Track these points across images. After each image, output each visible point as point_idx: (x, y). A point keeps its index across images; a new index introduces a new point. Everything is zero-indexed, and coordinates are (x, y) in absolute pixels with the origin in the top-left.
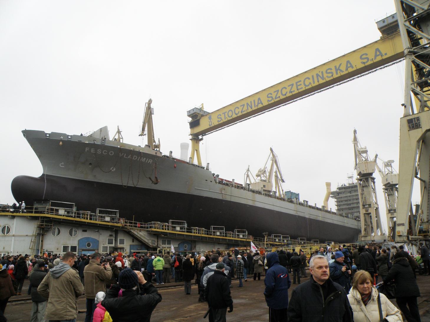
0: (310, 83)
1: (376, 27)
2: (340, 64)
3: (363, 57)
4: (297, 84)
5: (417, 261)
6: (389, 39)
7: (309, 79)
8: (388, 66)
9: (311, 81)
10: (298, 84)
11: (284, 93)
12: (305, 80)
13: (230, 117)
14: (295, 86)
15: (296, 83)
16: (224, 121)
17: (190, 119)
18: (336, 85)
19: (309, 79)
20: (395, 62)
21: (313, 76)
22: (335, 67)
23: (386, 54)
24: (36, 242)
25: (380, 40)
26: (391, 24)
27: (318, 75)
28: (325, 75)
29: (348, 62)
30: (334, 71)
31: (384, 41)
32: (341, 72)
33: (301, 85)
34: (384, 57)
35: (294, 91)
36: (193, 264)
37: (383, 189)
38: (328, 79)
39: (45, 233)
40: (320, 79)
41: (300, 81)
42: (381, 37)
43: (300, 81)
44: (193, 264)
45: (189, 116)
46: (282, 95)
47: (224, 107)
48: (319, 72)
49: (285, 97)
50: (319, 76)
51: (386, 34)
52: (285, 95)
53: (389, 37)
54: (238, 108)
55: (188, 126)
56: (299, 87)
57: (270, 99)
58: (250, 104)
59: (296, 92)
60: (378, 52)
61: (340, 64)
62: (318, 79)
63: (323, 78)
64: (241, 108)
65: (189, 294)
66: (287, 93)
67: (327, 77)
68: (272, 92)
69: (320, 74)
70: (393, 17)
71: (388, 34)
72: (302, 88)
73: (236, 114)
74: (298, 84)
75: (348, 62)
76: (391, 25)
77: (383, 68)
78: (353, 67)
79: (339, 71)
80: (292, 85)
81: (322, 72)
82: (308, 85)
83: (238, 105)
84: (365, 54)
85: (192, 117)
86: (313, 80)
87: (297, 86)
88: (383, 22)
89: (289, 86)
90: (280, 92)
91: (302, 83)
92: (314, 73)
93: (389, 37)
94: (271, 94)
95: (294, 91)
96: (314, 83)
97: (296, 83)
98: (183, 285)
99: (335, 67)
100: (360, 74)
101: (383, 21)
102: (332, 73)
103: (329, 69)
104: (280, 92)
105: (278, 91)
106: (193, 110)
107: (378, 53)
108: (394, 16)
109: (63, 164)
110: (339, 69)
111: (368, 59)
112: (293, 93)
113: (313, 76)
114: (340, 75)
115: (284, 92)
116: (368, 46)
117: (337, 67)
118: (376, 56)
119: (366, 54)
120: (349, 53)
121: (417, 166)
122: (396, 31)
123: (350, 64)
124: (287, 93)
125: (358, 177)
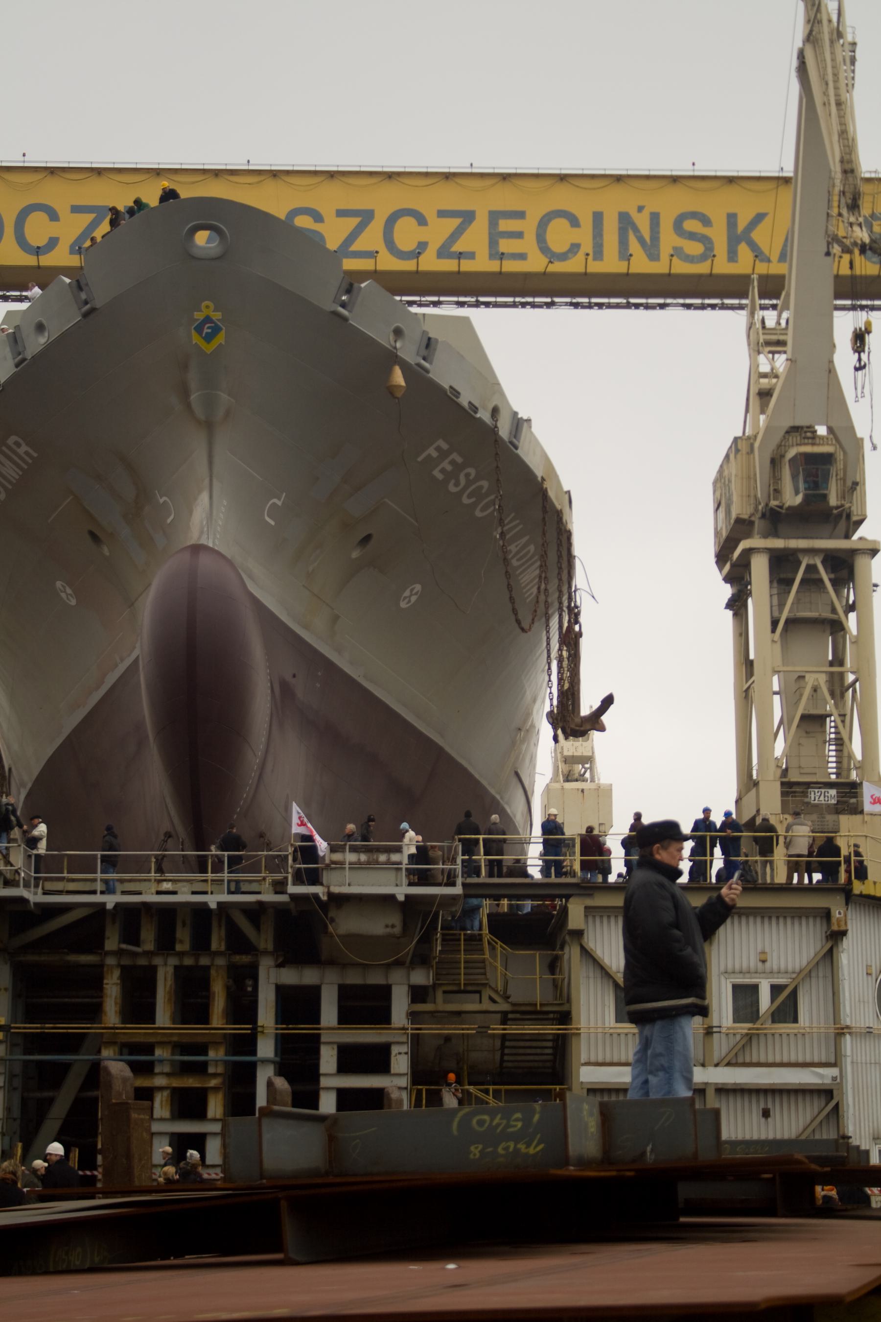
0: (575, 248)
2: (759, 218)
4: (497, 224)
5: (858, 887)
7: (574, 222)
9: (584, 236)
10: (505, 225)
11: (36, 238)
12: (549, 221)
14: (481, 225)
15: (495, 217)
16: (717, 270)
19: (574, 222)
20: (530, 300)
21: (598, 218)
22: (732, 219)
27: (626, 222)
28: (668, 240)
30: (719, 235)
32: (675, 259)
33: (519, 235)
35: (471, 256)
38: (681, 268)
40: (634, 246)
41: (520, 215)
43: (520, 215)
46: (544, 249)
48: (640, 209)
50: (636, 230)
52: (38, 251)
54: (422, 220)
56: (505, 246)
58: (643, 222)
59: (482, 264)
61: (759, 218)
62: (623, 243)
63: (652, 250)
64: (438, 231)
66: (53, 243)
67: (677, 252)
68: (327, 210)
69: (643, 222)
72: (522, 257)
73: (553, 257)
74: (505, 225)
77: (584, 307)
79: (743, 250)
80: (468, 217)
81: (655, 218)
82: (563, 257)
83: (430, 201)
84: (704, 215)
86: (594, 237)
87: (494, 237)
89: (341, 213)
90: (376, 229)
91: (529, 226)
92: (612, 204)
94: (318, 217)
95: (471, 256)
96: (598, 253)
97: (495, 217)
99: (732, 219)
100: (703, 297)
102: (706, 241)
103: (694, 215)
104: (376, 229)
105: (367, 216)
109: (818, 1188)
110: (746, 237)
112: (467, 266)
113: (598, 218)
115: (407, 234)
117: (741, 225)
121: (553, 614)
124: (53, 243)
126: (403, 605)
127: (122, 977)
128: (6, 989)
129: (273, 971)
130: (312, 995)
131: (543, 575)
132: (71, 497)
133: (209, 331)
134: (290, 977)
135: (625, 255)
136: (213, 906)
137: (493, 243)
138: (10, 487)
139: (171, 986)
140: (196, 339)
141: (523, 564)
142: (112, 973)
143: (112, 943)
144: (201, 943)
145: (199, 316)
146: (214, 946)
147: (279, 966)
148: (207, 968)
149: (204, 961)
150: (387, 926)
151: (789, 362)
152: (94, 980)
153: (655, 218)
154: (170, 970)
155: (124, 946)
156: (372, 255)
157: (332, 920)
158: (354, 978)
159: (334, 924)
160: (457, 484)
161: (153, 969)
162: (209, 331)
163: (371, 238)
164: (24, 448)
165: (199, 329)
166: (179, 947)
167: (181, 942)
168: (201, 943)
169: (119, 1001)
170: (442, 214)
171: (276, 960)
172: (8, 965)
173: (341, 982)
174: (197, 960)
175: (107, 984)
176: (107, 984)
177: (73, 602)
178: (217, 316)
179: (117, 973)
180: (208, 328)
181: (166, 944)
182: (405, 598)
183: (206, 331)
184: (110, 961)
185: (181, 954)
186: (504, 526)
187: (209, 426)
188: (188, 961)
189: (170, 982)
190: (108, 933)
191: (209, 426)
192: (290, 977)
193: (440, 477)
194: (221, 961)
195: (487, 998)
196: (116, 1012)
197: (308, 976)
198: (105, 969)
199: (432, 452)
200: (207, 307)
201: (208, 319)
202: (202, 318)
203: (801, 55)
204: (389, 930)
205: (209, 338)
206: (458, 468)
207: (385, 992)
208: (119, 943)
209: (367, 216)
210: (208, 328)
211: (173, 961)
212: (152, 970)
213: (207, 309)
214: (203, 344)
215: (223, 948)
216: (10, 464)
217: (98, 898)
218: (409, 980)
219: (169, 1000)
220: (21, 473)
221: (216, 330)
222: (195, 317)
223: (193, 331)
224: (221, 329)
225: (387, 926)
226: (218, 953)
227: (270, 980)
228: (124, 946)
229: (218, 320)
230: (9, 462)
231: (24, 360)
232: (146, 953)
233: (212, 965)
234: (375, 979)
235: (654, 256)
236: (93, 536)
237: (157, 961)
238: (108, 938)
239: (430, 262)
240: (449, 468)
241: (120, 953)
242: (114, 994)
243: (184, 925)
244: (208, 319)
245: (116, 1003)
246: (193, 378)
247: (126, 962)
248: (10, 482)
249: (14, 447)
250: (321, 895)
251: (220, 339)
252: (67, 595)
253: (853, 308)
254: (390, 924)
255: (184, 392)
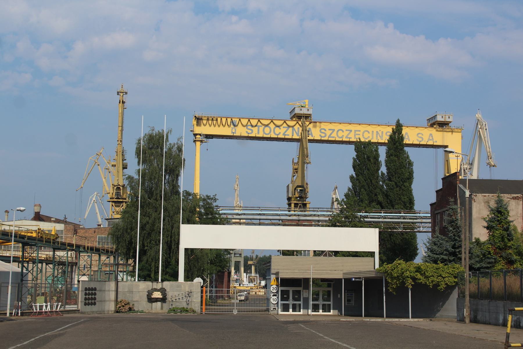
3: (420, 135)
7: (369, 132)
9: (370, 135)
10: (357, 133)
13: (339, 137)
14: (353, 131)
19: (369, 132)
21: (373, 132)
23: (436, 142)
24: (439, 211)
27: (377, 132)
35: (288, 135)
37: (354, 158)
40: (379, 138)
41: (360, 131)
43: (360, 131)
49: (276, 136)
52: (341, 137)
54: (343, 131)
57: (323, 135)
58: (380, 133)
62: (377, 136)
65: (486, 202)
66: (280, 133)
69: (380, 133)
74: (357, 133)
80: (351, 131)
81: (382, 132)
82: (367, 139)
89: (329, 130)
91: (361, 133)
94: (325, 130)
95: (288, 135)
96: (258, 133)
97: (355, 131)
107: (431, 138)
113: (373, 132)
115: (340, 134)
118: (429, 140)
119: (422, 135)
124: (280, 133)
125: (355, 157)
131: (69, 286)
135: (377, 138)
137: (355, 136)
151: (103, 289)
153: (382, 132)
156: (334, 137)
163: (334, 134)
170: (346, 130)
186: (127, 274)
203: (288, 186)
209: (334, 130)
235: (382, 139)
239: (345, 139)
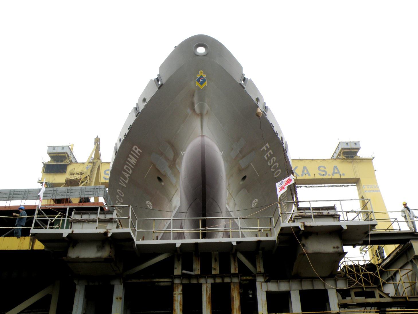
1: (46, 150)
2: (296, 167)
3: (321, 168)
6: (348, 162)
8: (336, 187)
17: (48, 159)
18: (329, 186)
25: (329, 159)
26: (59, 153)
29: (305, 168)
31: (343, 162)
34: (342, 177)
36: (339, 269)
39: (416, 260)
42: (48, 161)
44: (339, 269)
45: (49, 153)
47: (301, 160)
51: (54, 161)
53: (348, 160)
55: (40, 167)
60: (305, 170)
61: (296, 167)
70: (63, 148)
71: (347, 157)
75: (305, 168)
76: (60, 155)
78: (309, 175)
85: (52, 157)
88: (61, 148)
93: (348, 160)
98: (29, 248)
101: (54, 148)
106: (63, 148)
107: (336, 171)
108: (55, 148)
111: (326, 173)
114: (313, 178)
116: (327, 161)
119: (325, 168)
120: (295, 160)
122: (62, 162)
123: (307, 170)
126: (253, 206)
127: (183, 290)
128: (121, 298)
129: (264, 285)
130: (286, 295)
132: (152, 165)
133: (202, 81)
134: (273, 287)
136: (235, 244)
138: (133, 167)
139: (210, 294)
140: (197, 84)
141: (284, 198)
142: (178, 288)
143: (178, 271)
144: (225, 271)
145: (198, 76)
146: (233, 271)
147: (267, 281)
148: (229, 284)
149: (227, 280)
150: (334, 248)
152: (170, 290)
154: (209, 286)
155: (185, 272)
157: (304, 245)
158: (307, 286)
159: (305, 247)
160: (270, 163)
161: (200, 286)
162: (202, 81)
164: (138, 150)
165: (198, 81)
166: (214, 272)
167: (215, 269)
168: (225, 271)
169: (182, 303)
171: (264, 279)
172: (122, 285)
173: (300, 289)
174: (223, 280)
175: (175, 294)
176: (175, 294)
177: (152, 207)
178: (204, 76)
179: (180, 288)
180: (201, 80)
181: (206, 272)
182: (253, 203)
183: (201, 81)
184: (177, 281)
185: (214, 277)
187: (201, 115)
188: (218, 281)
189: (209, 292)
190: (176, 266)
191: (201, 115)
192: (273, 287)
193: (266, 158)
194: (236, 280)
195: (378, 295)
196: (180, 309)
197: (283, 287)
198: (174, 286)
199: (264, 148)
200: (201, 72)
201: (201, 77)
202: (199, 77)
204: (336, 250)
205: (202, 84)
206: (272, 156)
207: (324, 294)
208: (182, 269)
210: (201, 80)
211: (210, 281)
212: (199, 286)
213: (201, 73)
214: (199, 86)
215: (237, 272)
216: (134, 158)
217: (171, 241)
218: (336, 286)
219: (209, 302)
220: (136, 160)
221: (204, 81)
222: (197, 76)
223: (196, 82)
224: (206, 80)
225: (334, 248)
226: (235, 275)
227: (262, 290)
228: (185, 272)
229: (205, 77)
230: (133, 157)
231: (139, 113)
232: (197, 277)
233: (231, 282)
234: (318, 286)
236: (159, 179)
237: (202, 281)
238: (176, 268)
240: (269, 156)
241: (182, 276)
242: (179, 300)
243: (216, 261)
244: (201, 77)
245: (180, 305)
246: (196, 99)
247: (185, 282)
248: (134, 163)
249: (135, 150)
250: (300, 227)
251: (205, 84)
252: (149, 205)
253: (351, 149)
254: (336, 246)
255: (193, 105)
